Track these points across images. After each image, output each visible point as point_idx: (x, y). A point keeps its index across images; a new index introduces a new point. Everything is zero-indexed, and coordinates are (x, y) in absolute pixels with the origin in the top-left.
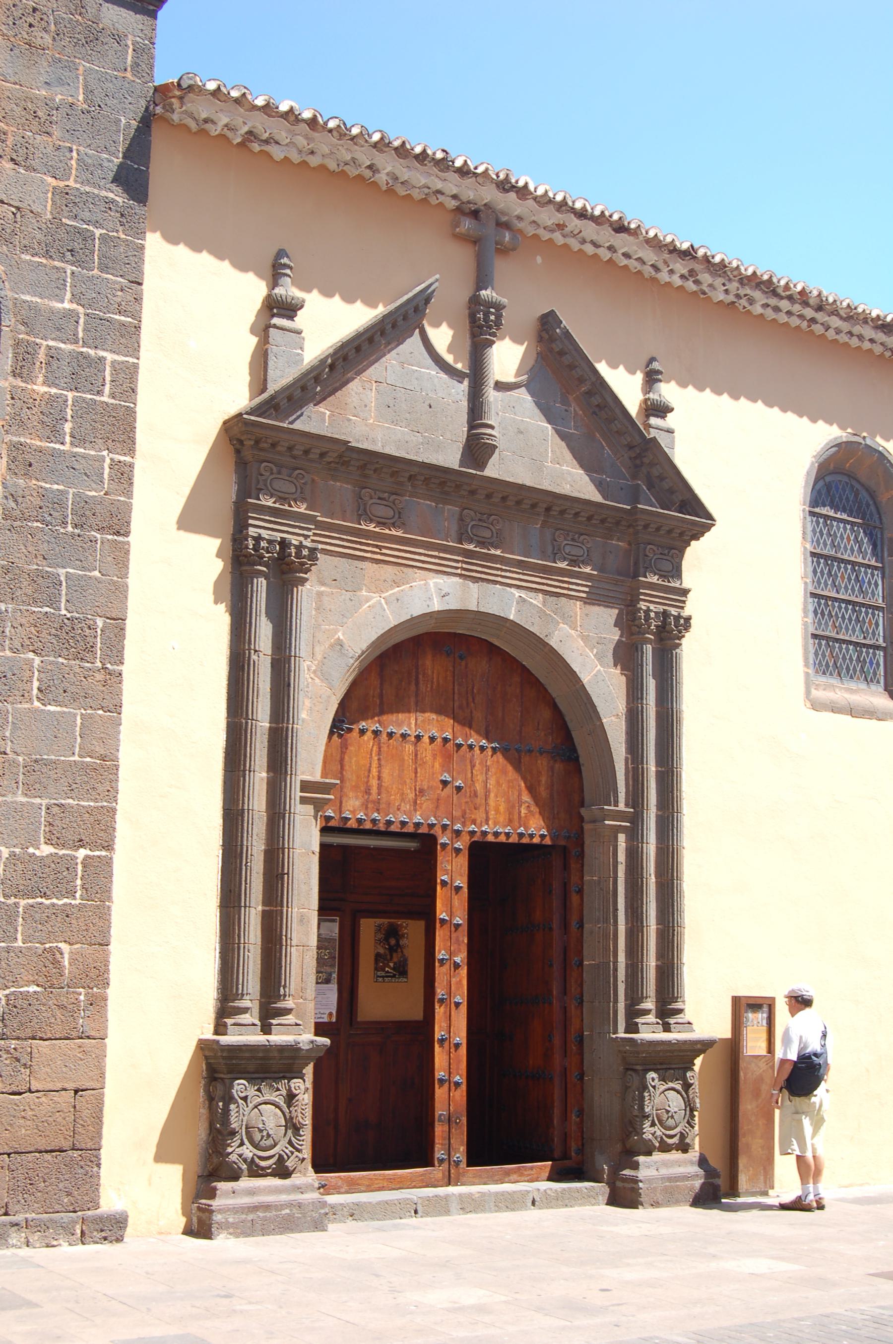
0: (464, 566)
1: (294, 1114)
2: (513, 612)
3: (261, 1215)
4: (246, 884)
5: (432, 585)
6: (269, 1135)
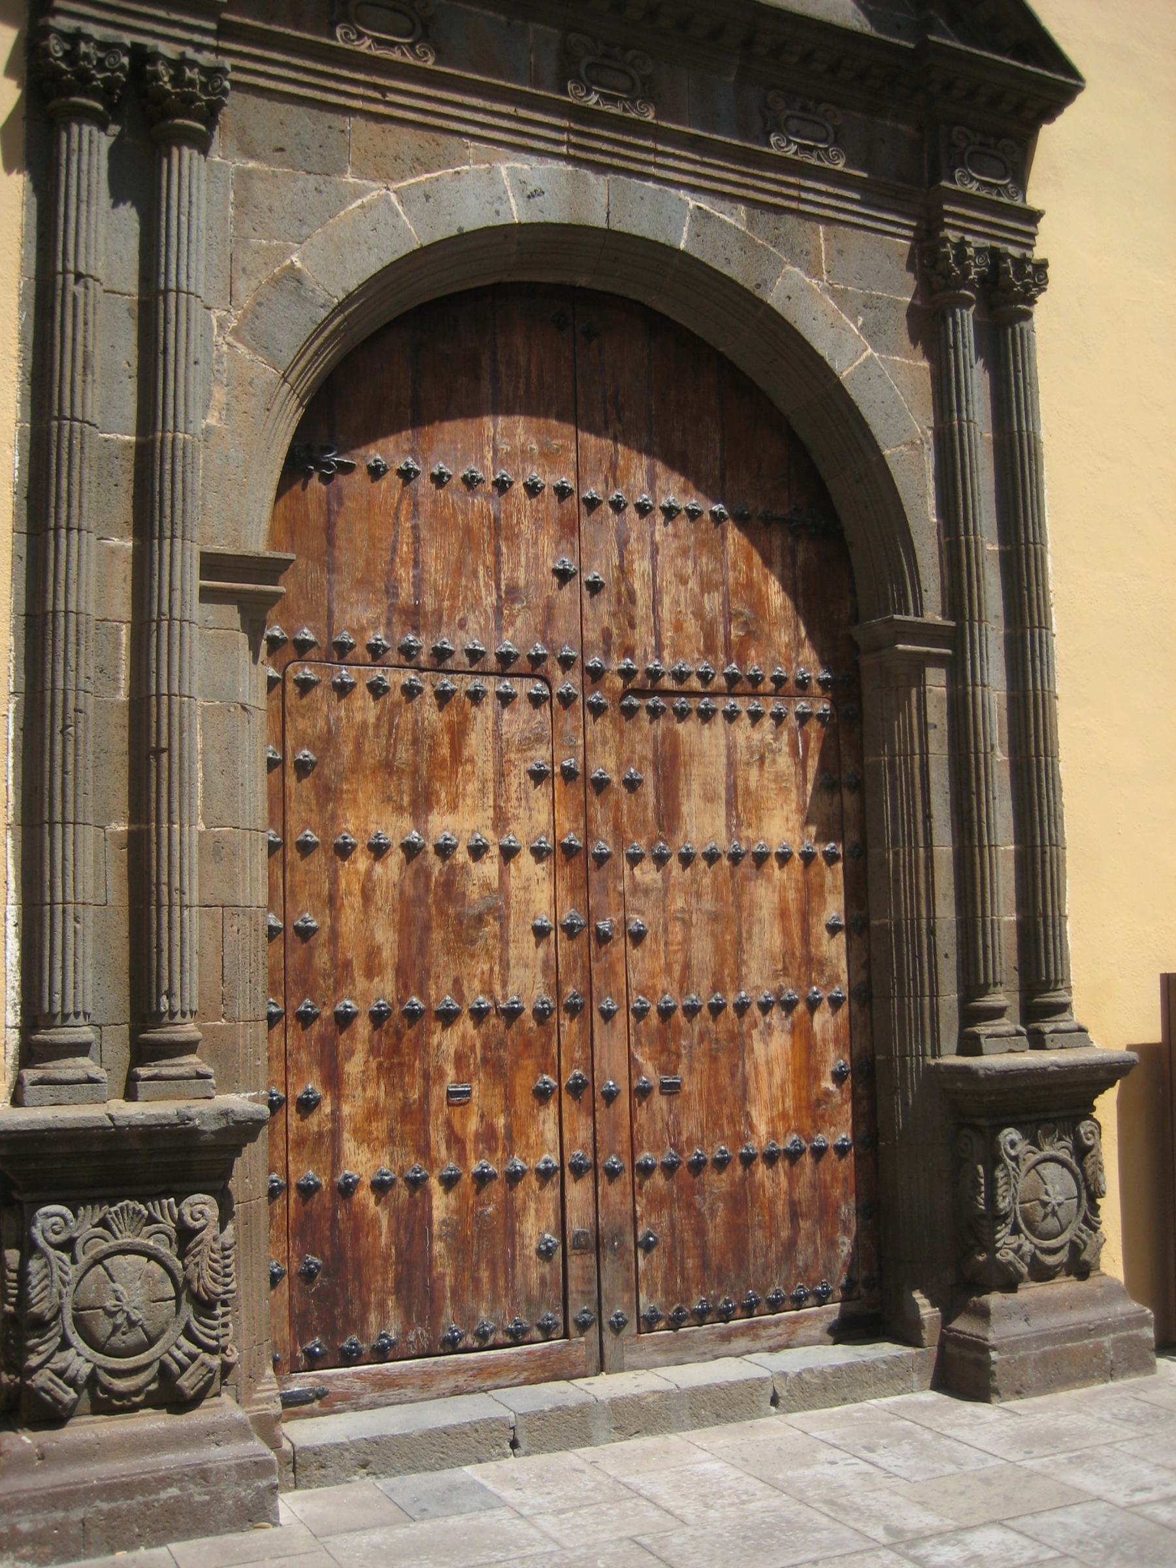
0: (574, 139)
1: (193, 1272)
2: (685, 236)
3: (105, 1506)
4: (65, 772)
5: (504, 172)
6: (132, 1324)
